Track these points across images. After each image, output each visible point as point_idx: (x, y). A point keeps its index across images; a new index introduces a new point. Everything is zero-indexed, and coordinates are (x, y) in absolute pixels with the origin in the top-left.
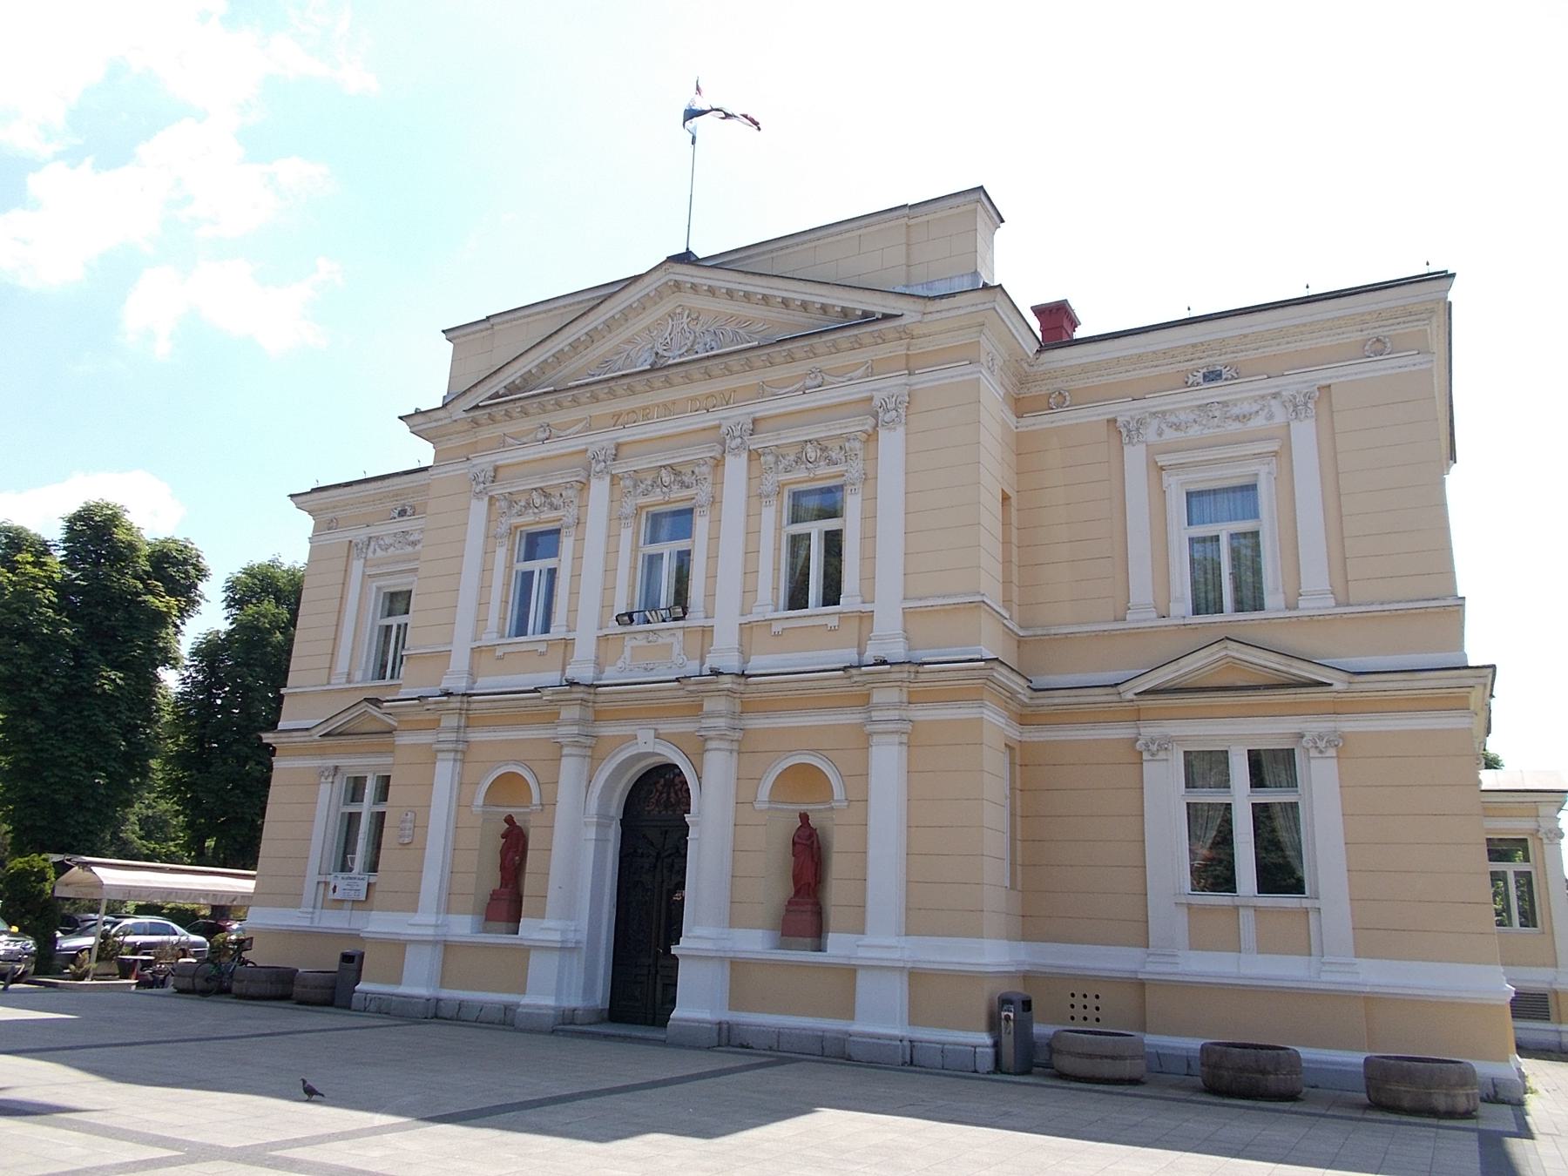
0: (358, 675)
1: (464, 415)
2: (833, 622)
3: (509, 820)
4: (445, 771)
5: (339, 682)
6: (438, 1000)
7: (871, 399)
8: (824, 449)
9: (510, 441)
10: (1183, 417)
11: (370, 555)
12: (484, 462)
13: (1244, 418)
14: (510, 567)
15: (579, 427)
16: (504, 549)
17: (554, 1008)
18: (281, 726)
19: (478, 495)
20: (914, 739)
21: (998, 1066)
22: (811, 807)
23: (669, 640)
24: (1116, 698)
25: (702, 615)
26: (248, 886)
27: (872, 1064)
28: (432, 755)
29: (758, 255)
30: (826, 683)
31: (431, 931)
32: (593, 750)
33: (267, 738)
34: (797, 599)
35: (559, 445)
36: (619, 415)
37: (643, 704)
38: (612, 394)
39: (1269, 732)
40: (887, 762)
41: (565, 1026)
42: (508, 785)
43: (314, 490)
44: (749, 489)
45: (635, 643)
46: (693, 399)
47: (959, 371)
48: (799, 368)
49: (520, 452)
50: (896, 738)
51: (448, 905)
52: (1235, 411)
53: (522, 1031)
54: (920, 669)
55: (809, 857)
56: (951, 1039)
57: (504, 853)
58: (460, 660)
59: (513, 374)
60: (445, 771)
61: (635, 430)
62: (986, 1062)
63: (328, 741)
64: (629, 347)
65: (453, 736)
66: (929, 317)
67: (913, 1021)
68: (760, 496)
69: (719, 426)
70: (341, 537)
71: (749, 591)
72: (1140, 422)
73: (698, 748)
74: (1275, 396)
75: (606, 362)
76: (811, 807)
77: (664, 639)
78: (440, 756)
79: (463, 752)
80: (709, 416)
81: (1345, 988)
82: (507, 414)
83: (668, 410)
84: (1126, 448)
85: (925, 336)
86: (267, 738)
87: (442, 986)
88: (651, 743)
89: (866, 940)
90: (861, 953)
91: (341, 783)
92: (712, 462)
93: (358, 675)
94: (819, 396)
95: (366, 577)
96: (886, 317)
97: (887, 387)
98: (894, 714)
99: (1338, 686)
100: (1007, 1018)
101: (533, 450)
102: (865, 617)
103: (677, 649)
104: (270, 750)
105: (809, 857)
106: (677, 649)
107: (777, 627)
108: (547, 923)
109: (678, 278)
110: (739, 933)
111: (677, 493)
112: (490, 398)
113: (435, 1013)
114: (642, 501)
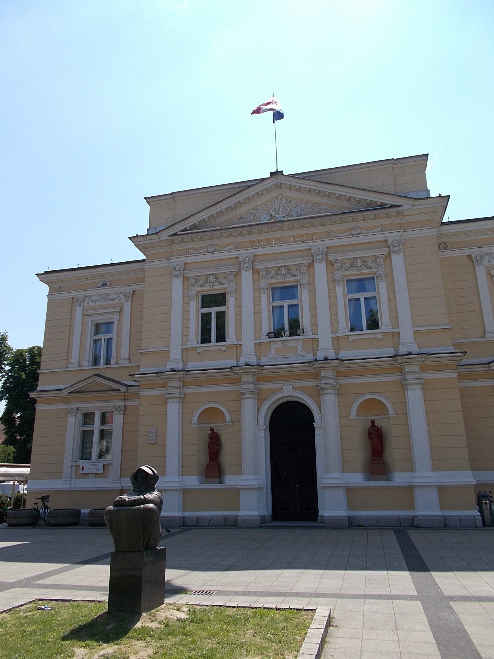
0: (85, 363)
1: (168, 238)
2: (224, 348)
3: (212, 430)
4: (174, 409)
5: (74, 366)
6: (184, 518)
7: (310, 249)
8: (364, 262)
9: (192, 251)
10: (95, 298)
11: (86, 304)
12: (178, 261)
13: (112, 300)
14: (197, 311)
15: (232, 246)
16: (266, 295)
17: (259, 516)
18: (39, 388)
19: (176, 276)
20: (425, 386)
21: (484, 524)
22: (375, 417)
23: (295, 344)
24: (61, 395)
25: (311, 333)
26: (26, 470)
27: (430, 528)
28: (165, 401)
29: (320, 175)
30: (370, 364)
31: (178, 484)
32: (260, 397)
33: (32, 395)
34: (205, 339)
35: (219, 255)
36: (253, 242)
37: (286, 373)
38: (251, 233)
39: (107, 405)
40: (415, 397)
41: (262, 524)
42: (210, 413)
43: (46, 273)
44: (253, 286)
45: (276, 346)
46: (294, 237)
47: (427, 231)
48: (348, 226)
49: (199, 257)
50: (418, 386)
51: (183, 471)
52: (110, 297)
53: (242, 528)
54: (188, 373)
55: (376, 438)
56: (462, 514)
57: (210, 446)
58: (273, 346)
59: (195, 220)
60: (174, 409)
61: (264, 249)
62: (480, 523)
63: (71, 396)
64: (255, 212)
65: (177, 391)
66: (414, 208)
67: (184, 510)
68: (334, 281)
69: (238, 257)
70: (67, 296)
71: (185, 336)
72: (482, 257)
73: (318, 393)
74: (122, 293)
75: (241, 218)
76: (375, 417)
77: (292, 344)
78: (170, 400)
79: (182, 398)
80: (303, 245)
81: (455, 484)
82: (192, 239)
83: (280, 241)
84: (476, 267)
85: (409, 215)
86: (32, 395)
87: (184, 510)
88: (289, 392)
89: (417, 474)
90: (416, 480)
91: (80, 416)
92: (307, 265)
93: (85, 363)
94: (359, 238)
95: (85, 316)
96: (393, 206)
97: (392, 236)
98: (417, 376)
99: (123, 390)
100: (486, 503)
101: (206, 256)
102: (238, 347)
103: (300, 348)
104: (34, 401)
105: (376, 438)
106: (300, 348)
107: (199, 350)
108: (246, 477)
109: (281, 182)
110: (347, 475)
111: (289, 278)
112: (181, 231)
113: (352, 524)
114: (200, 289)
